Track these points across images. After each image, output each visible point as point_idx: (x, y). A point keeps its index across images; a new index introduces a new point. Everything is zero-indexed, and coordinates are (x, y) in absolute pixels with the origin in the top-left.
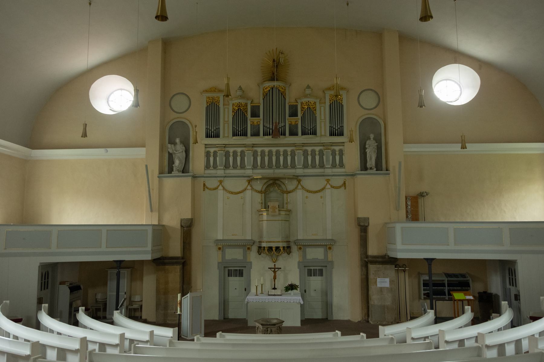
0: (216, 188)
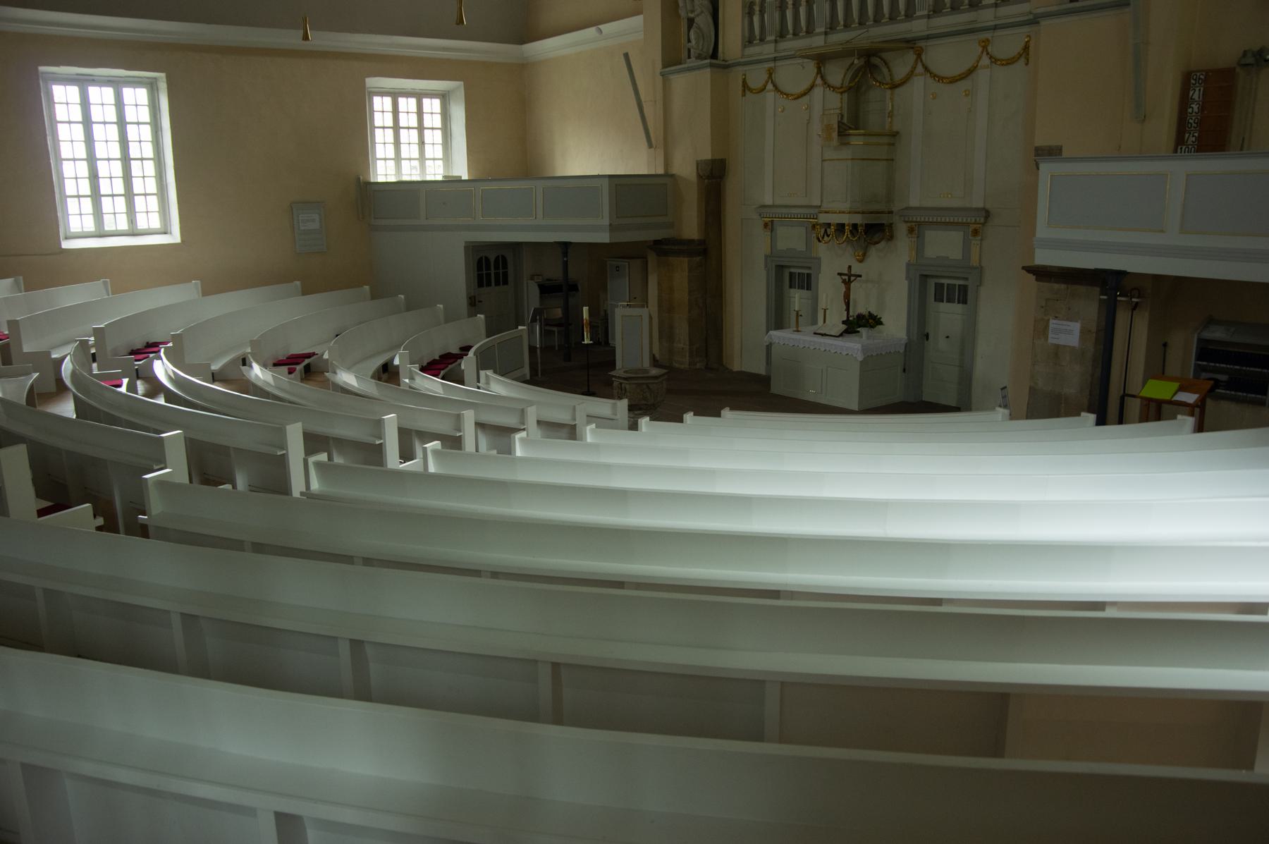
0: (763, 89)
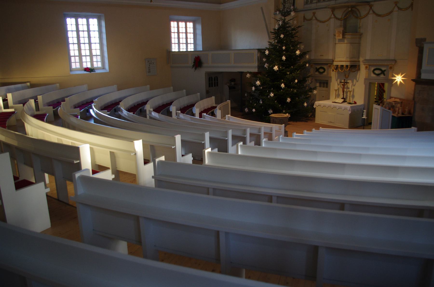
0: (311, 20)
